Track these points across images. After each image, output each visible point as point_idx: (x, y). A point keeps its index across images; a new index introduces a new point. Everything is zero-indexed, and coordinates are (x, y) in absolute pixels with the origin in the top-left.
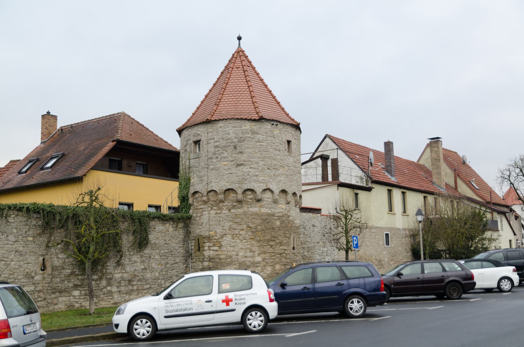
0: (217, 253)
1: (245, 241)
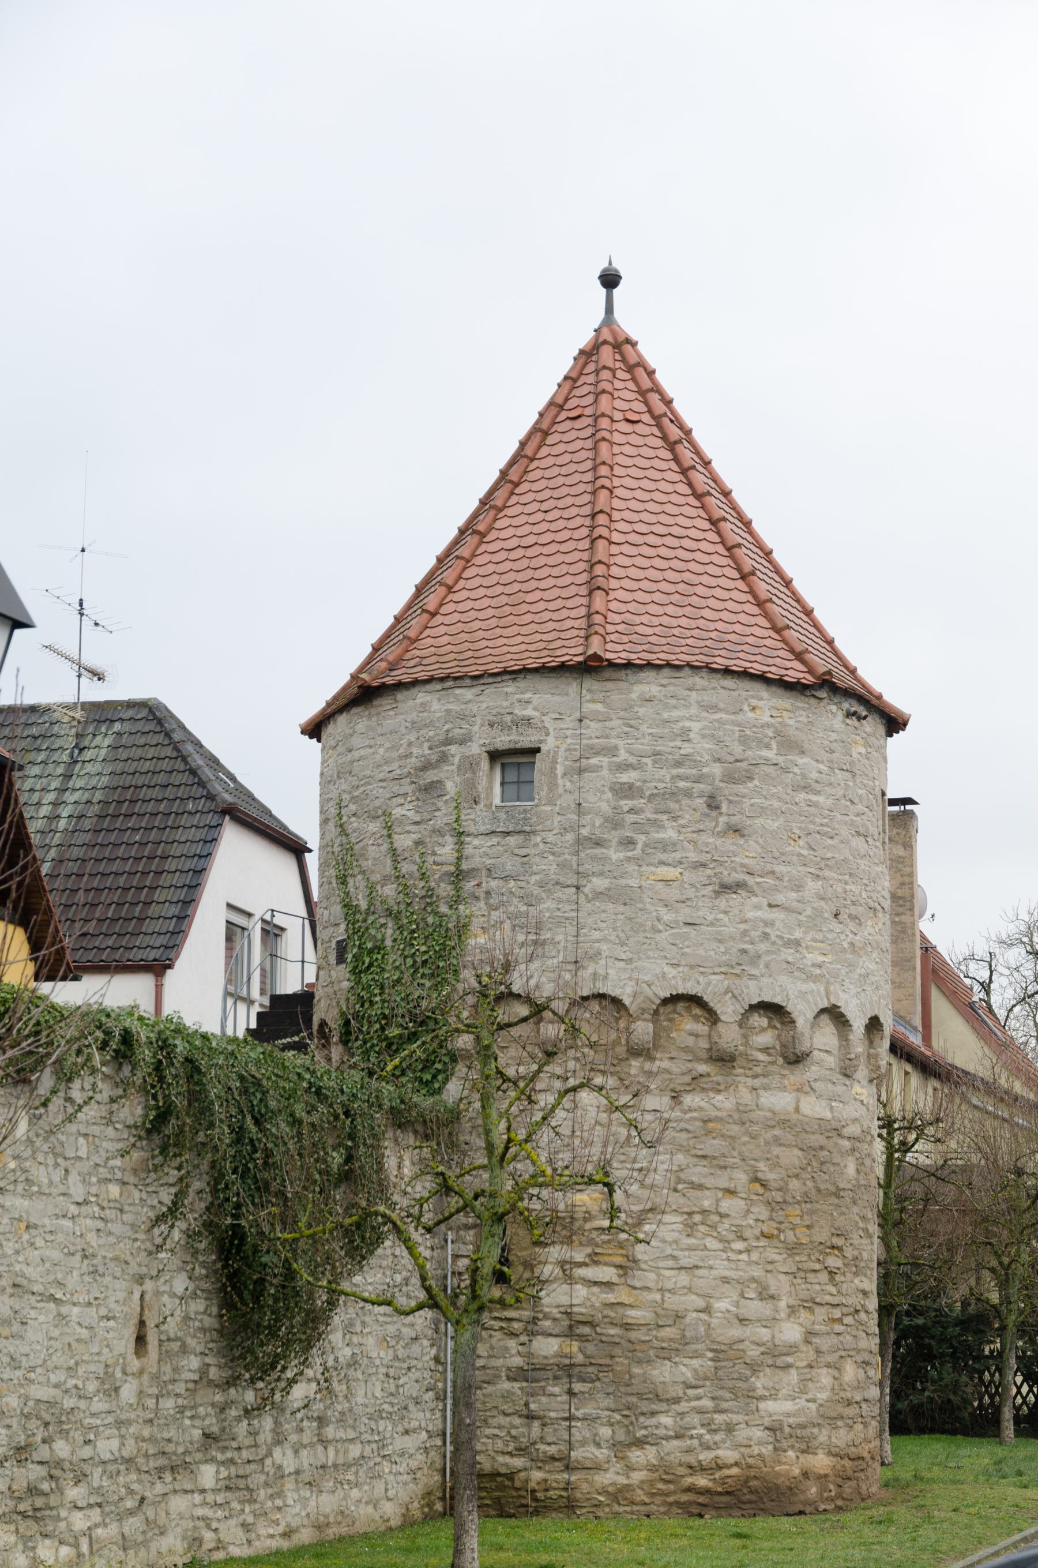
0: (611, 1298)
1: (739, 1245)
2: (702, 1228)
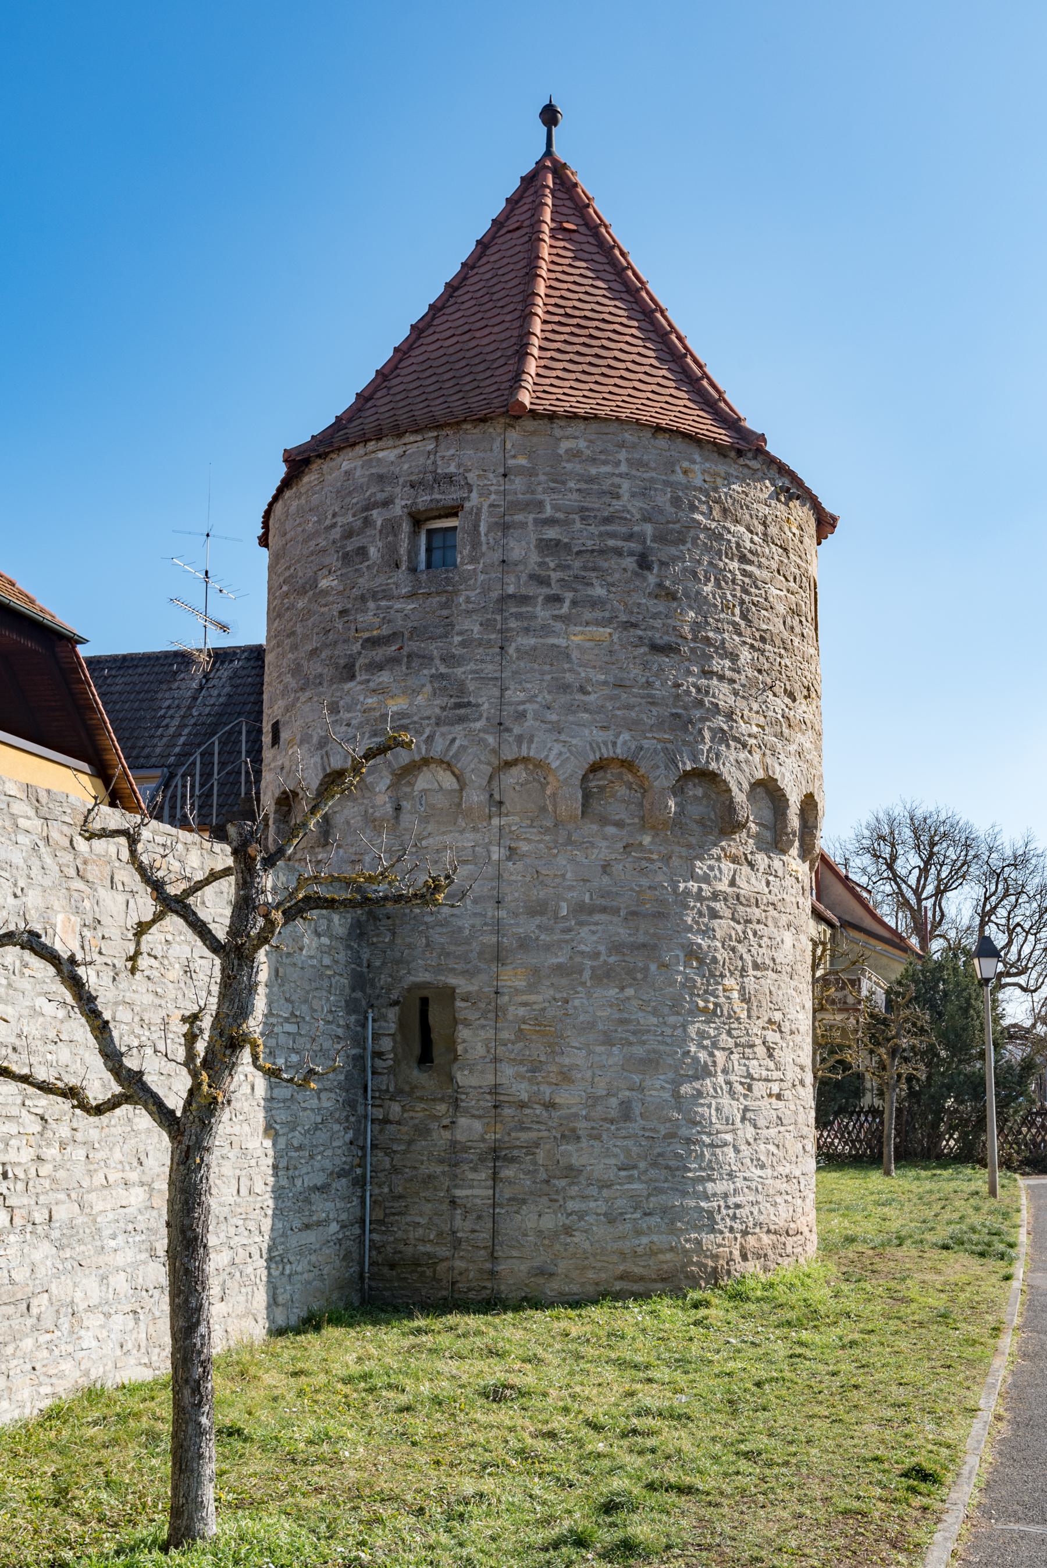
2: (635, 1003)
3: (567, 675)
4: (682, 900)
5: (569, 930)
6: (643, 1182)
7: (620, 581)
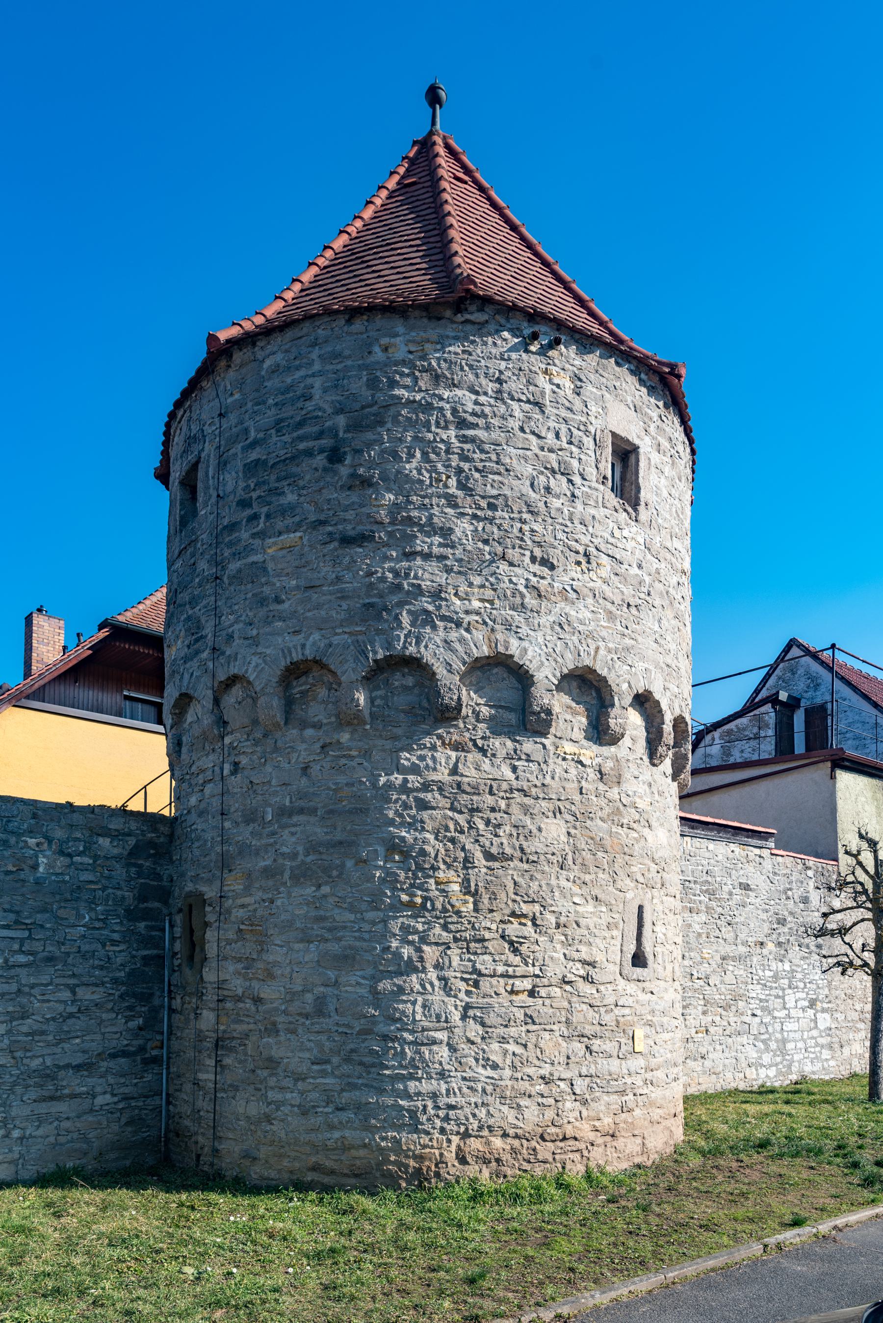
3: (265, 589)
4: (383, 794)
5: (273, 833)
6: (336, 1077)
7: (310, 481)
